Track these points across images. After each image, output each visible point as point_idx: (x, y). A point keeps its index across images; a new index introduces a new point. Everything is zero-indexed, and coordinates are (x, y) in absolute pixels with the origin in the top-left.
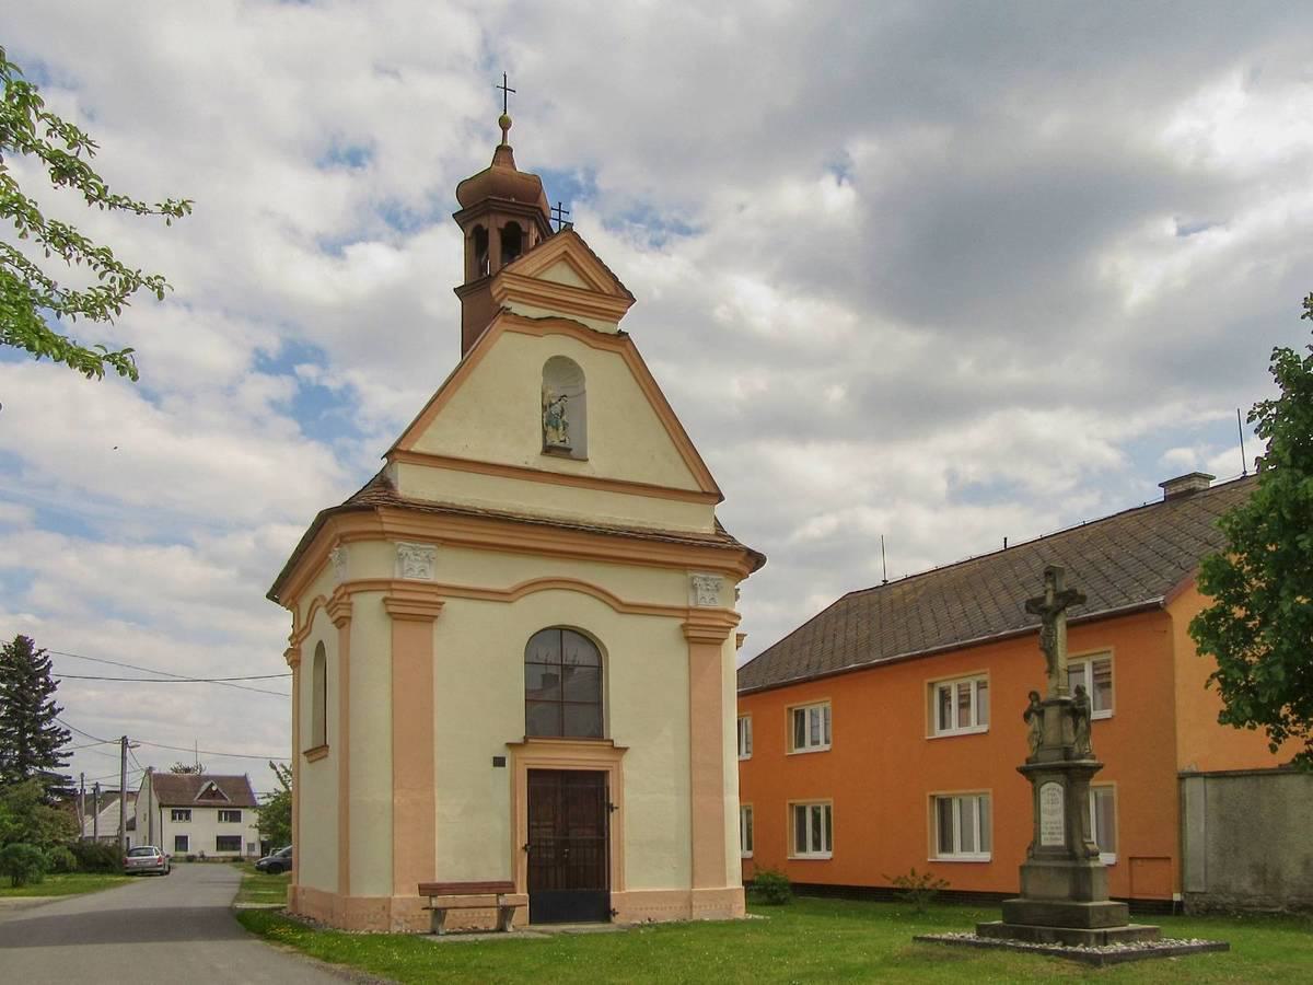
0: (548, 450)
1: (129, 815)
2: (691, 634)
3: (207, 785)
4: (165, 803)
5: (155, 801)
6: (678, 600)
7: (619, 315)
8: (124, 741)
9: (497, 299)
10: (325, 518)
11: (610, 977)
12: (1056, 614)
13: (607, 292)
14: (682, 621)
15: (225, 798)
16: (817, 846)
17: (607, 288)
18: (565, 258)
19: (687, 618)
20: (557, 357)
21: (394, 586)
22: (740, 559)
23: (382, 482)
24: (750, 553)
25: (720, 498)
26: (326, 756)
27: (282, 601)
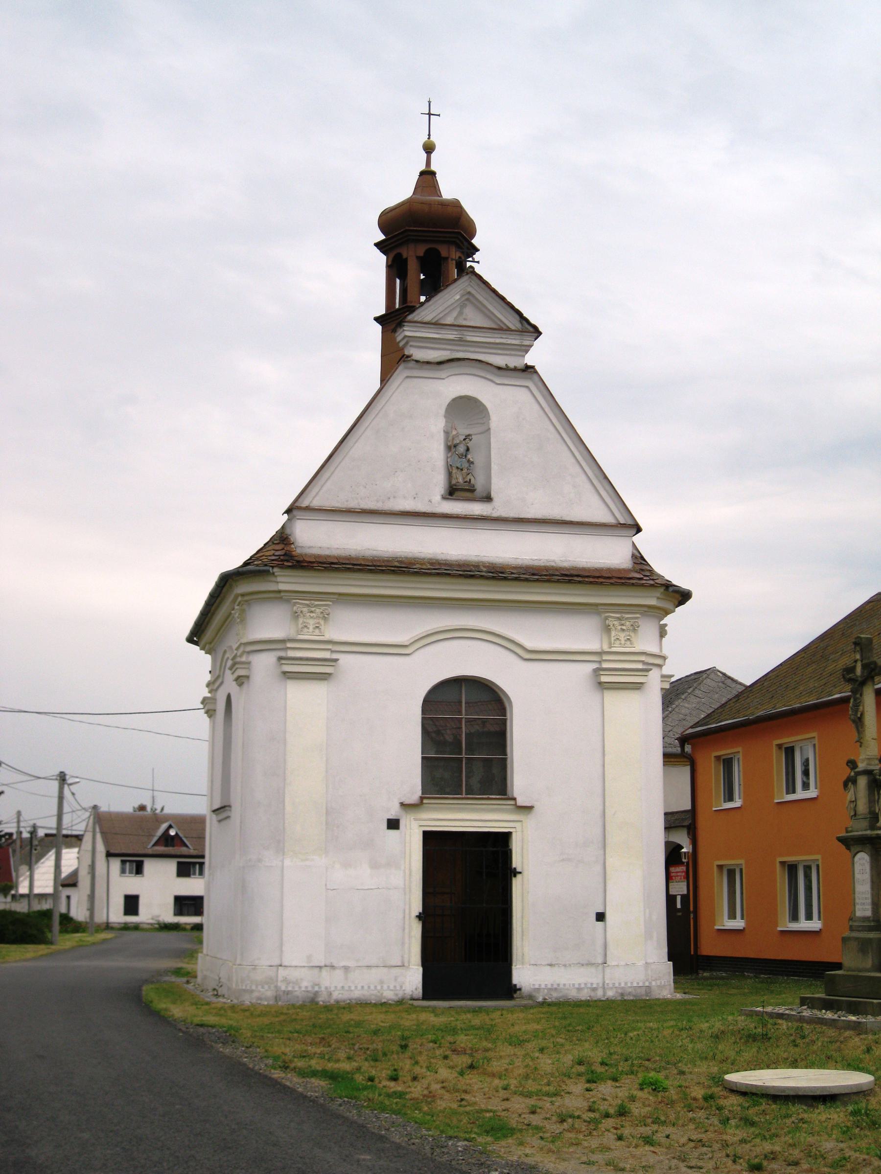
0: (452, 492)
1: (66, 871)
2: (604, 679)
3: (164, 826)
4: (112, 851)
5: (101, 848)
6: (593, 644)
7: (527, 349)
8: (62, 778)
9: (401, 344)
10: (226, 581)
11: (675, 1113)
12: (863, 683)
13: (513, 328)
14: (595, 666)
15: (186, 846)
16: (809, 917)
17: (512, 322)
18: (469, 298)
19: (600, 662)
20: (461, 398)
21: (289, 645)
22: (658, 595)
23: (282, 538)
24: (668, 586)
25: (639, 530)
26: (228, 817)
27: (202, 643)
